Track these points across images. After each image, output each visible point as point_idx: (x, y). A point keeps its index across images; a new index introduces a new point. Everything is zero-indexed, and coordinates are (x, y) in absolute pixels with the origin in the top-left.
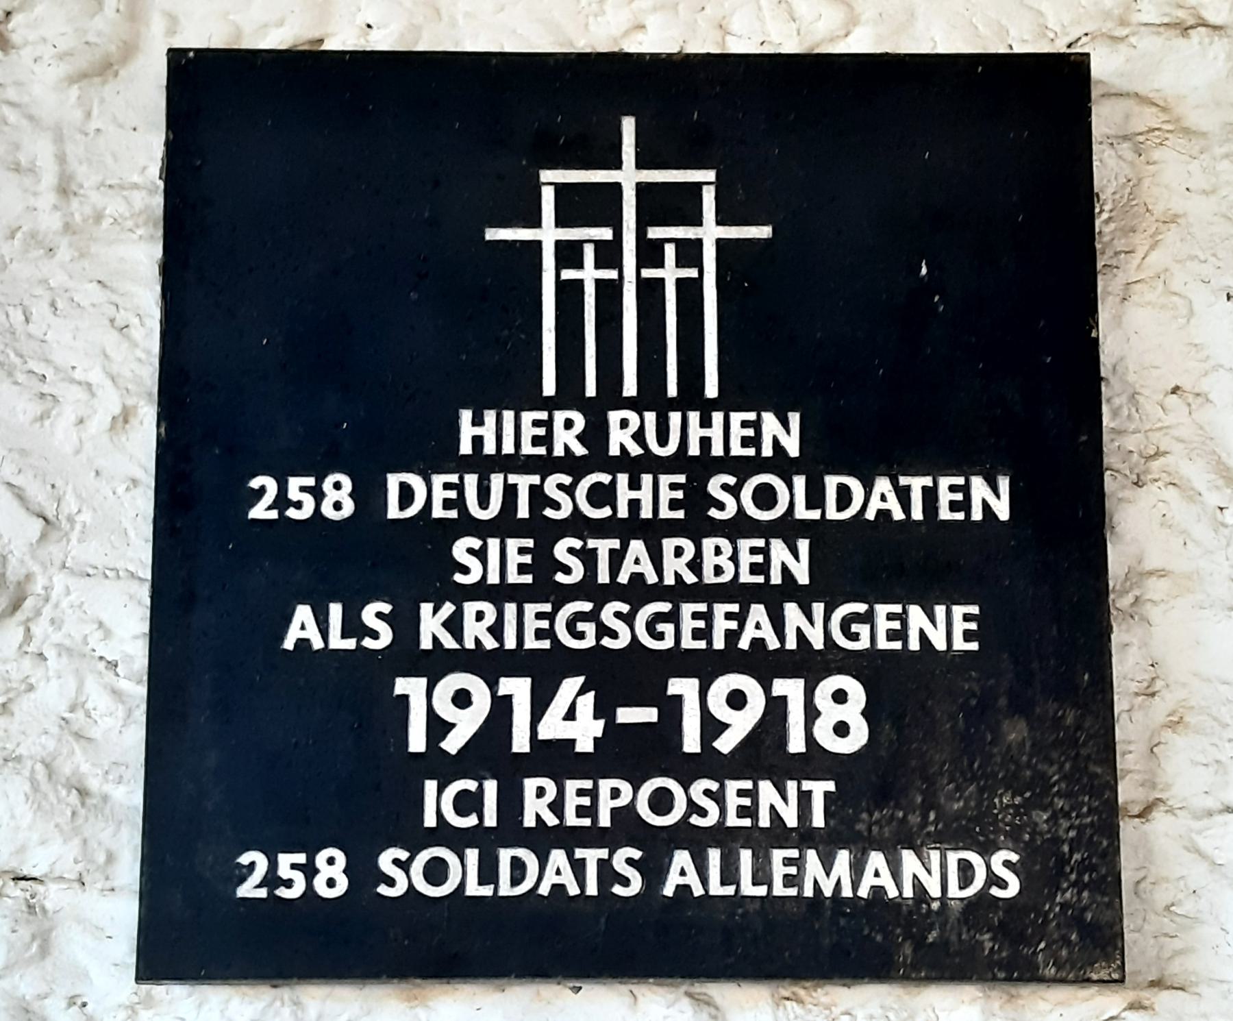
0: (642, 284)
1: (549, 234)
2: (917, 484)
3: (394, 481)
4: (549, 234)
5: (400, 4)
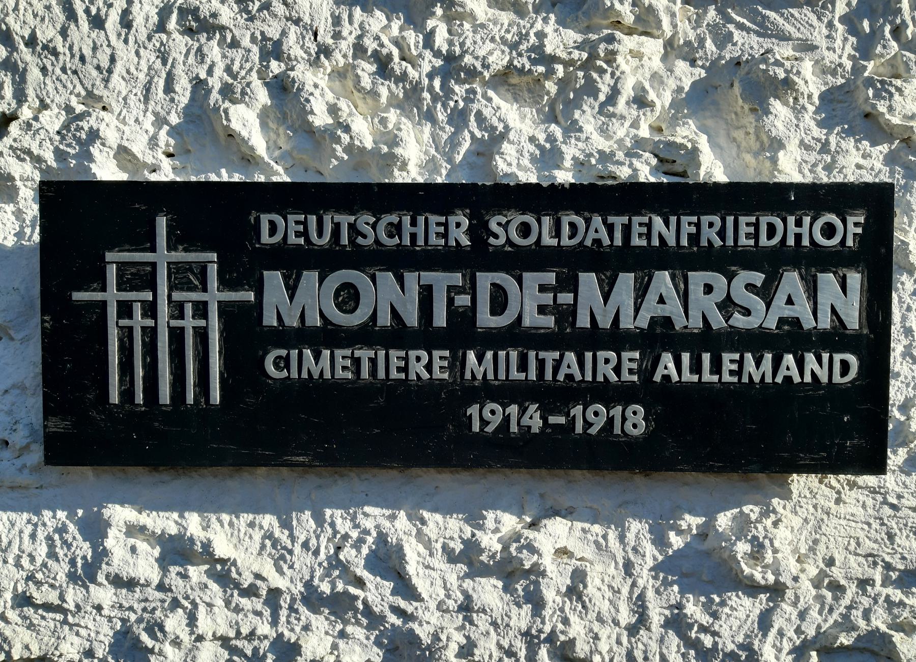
0: (172, 330)
1: (112, 295)
2: (618, 221)
3: (265, 219)
4: (112, 295)
5: (85, 2)
